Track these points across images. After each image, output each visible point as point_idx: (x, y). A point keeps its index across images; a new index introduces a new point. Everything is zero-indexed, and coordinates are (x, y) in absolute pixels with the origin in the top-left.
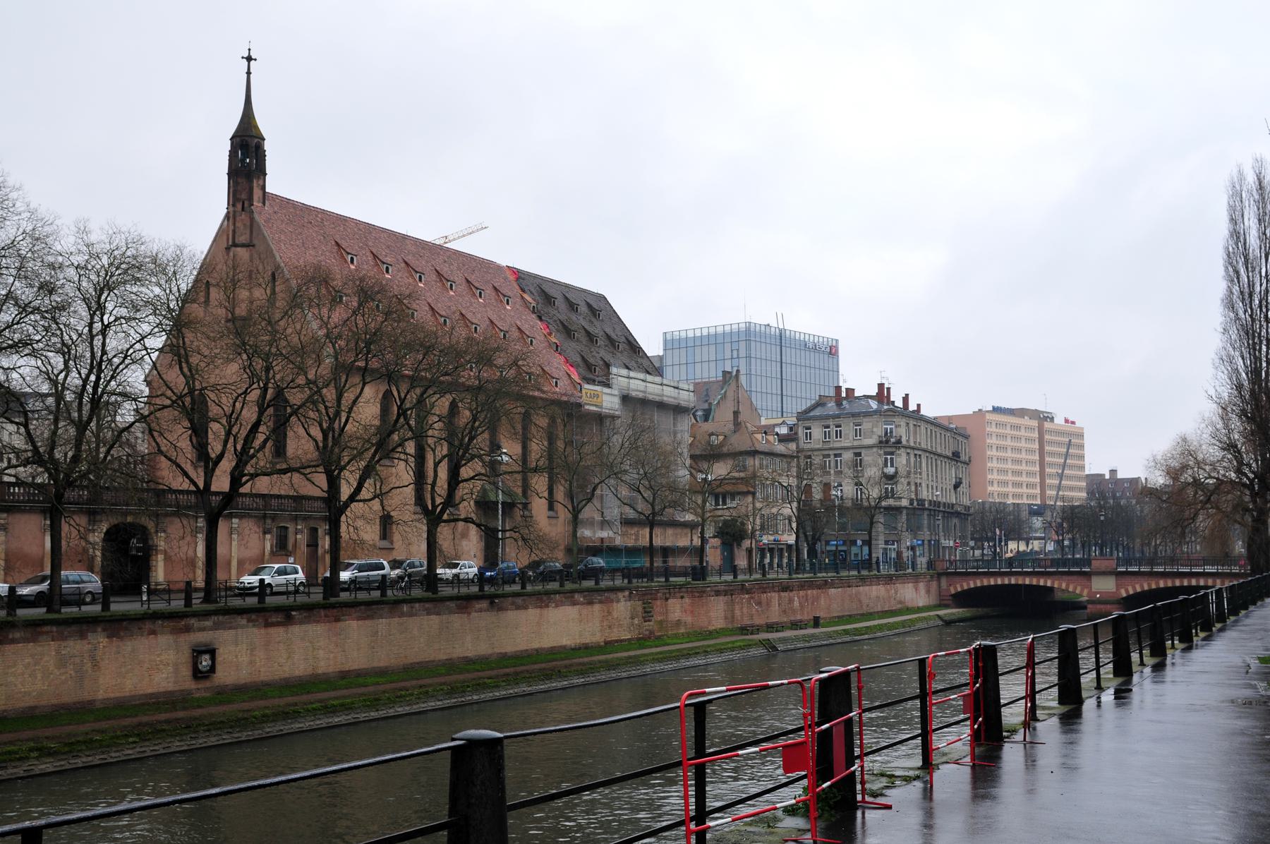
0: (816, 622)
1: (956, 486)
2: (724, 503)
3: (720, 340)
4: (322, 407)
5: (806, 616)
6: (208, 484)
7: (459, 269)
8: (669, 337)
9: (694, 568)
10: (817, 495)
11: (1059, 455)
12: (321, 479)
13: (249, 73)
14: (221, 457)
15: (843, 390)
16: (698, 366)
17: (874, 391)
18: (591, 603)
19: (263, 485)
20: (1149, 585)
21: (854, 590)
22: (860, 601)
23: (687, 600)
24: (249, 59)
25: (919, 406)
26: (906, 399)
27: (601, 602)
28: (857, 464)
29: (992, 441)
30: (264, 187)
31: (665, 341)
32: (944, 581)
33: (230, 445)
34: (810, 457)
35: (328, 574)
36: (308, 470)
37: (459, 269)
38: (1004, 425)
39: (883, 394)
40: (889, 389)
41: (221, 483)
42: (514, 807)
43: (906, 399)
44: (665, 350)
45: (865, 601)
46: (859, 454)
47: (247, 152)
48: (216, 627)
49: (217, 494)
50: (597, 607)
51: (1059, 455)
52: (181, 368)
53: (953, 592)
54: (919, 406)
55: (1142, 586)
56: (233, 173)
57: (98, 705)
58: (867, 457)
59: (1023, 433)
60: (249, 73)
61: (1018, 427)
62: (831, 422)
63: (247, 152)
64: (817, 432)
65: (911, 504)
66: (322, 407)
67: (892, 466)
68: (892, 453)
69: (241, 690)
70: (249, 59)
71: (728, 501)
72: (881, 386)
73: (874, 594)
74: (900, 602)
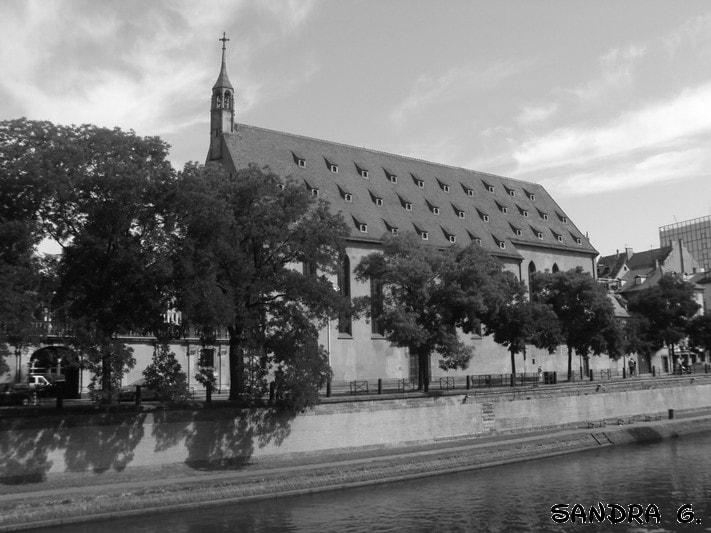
13: (224, 49)
31: (661, 233)
60: (224, 49)
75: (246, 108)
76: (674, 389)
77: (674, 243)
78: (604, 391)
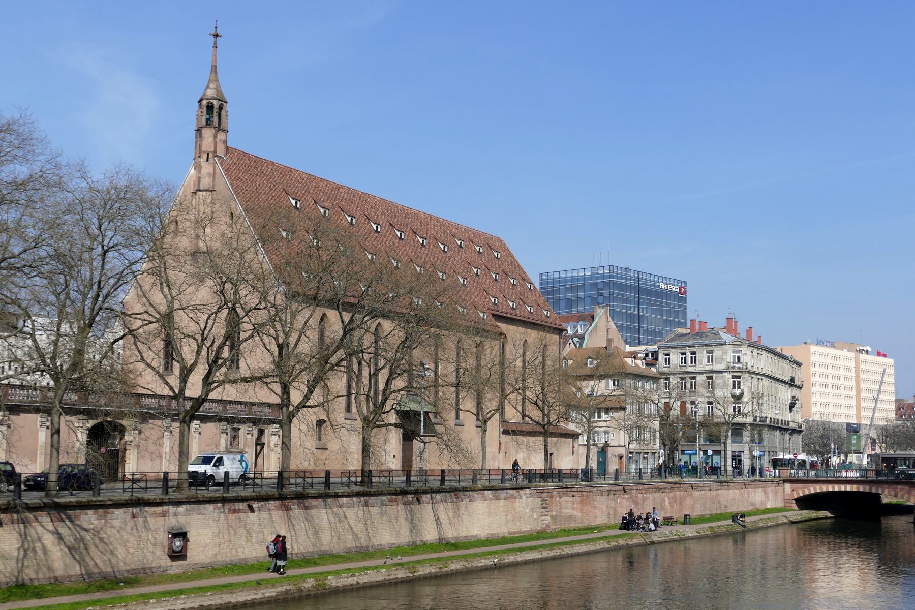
0: (687, 520)
1: (792, 406)
2: (600, 417)
4: (279, 327)
5: (678, 515)
6: (182, 391)
7: (383, 214)
8: (544, 277)
10: (675, 412)
11: (874, 382)
12: (278, 388)
14: (194, 364)
15: (697, 322)
18: (497, 498)
19: (230, 392)
20: (815, 489)
21: (714, 493)
22: (719, 503)
24: (216, 35)
25: (760, 337)
27: (506, 498)
28: (711, 385)
29: (816, 369)
30: (225, 142)
32: (788, 486)
33: (204, 352)
34: (694, 378)
35: (885, 500)
36: (268, 380)
37: (383, 214)
38: (826, 355)
41: (194, 389)
45: (724, 503)
46: (710, 378)
47: (213, 112)
48: (187, 513)
49: (190, 399)
50: (502, 502)
51: (874, 382)
52: (162, 288)
54: (760, 337)
55: (803, 491)
58: (718, 379)
59: (841, 363)
61: (837, 358)
62: (687, 350)
64: (676, 358)
65: (755, 420)
66: (279, 327)
67: (739, 388)
68: (739, 377)
69: (214, 570)
71: (603, 414)
72: (729, 319)
73: (731, 496)
74: (752, 504)
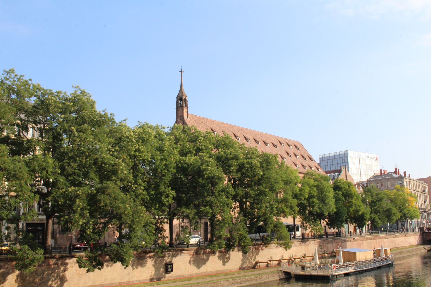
3: (336, 157)
9: (336, 233)
13: (181, 76)
16: (334, 165)
17: (393, 171)
23: (334, 244)
25: (409, 175)
26: (405, 173)
31: (320, 158)
37: (251, 135)
39: (396, 171)
40: (399, 170)
42: (346, 179)
43: (405, 173)
44: (320, 161)
47: (181, 101)
53: (428, 239)
54: (409, 175)
56: (177, 108)
57: (135, 282)
60: (181, 76)
63: (181, 101)
70: (181, 72)
72: (396, 169)
75: (193, 110)
76: (377, 240)
77: (342, 168)
78: (355, 241)
